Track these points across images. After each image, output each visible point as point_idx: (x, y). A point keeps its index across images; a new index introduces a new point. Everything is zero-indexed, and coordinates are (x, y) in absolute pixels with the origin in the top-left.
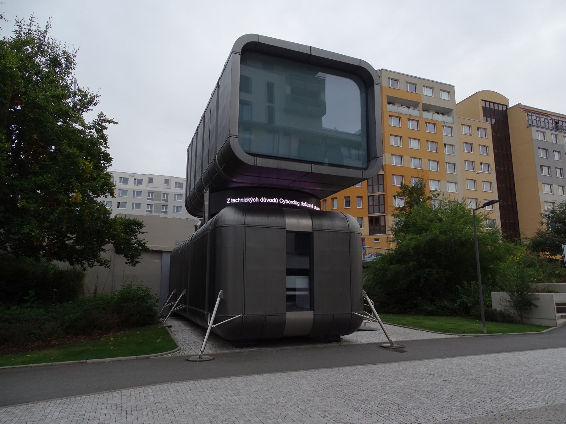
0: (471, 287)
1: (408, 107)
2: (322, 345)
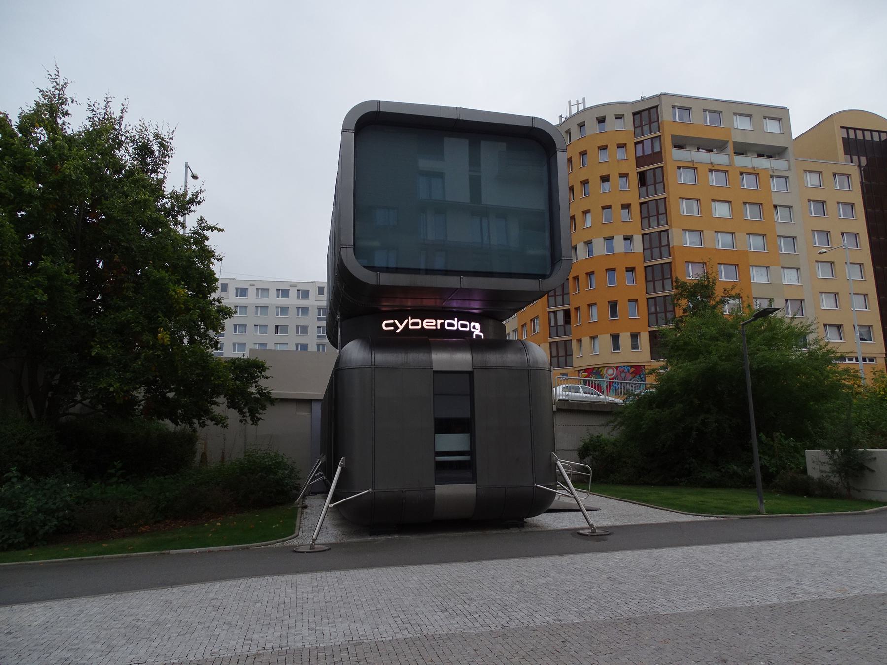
0: (773, 441)
1: (709, 150)
2: (494, 532)
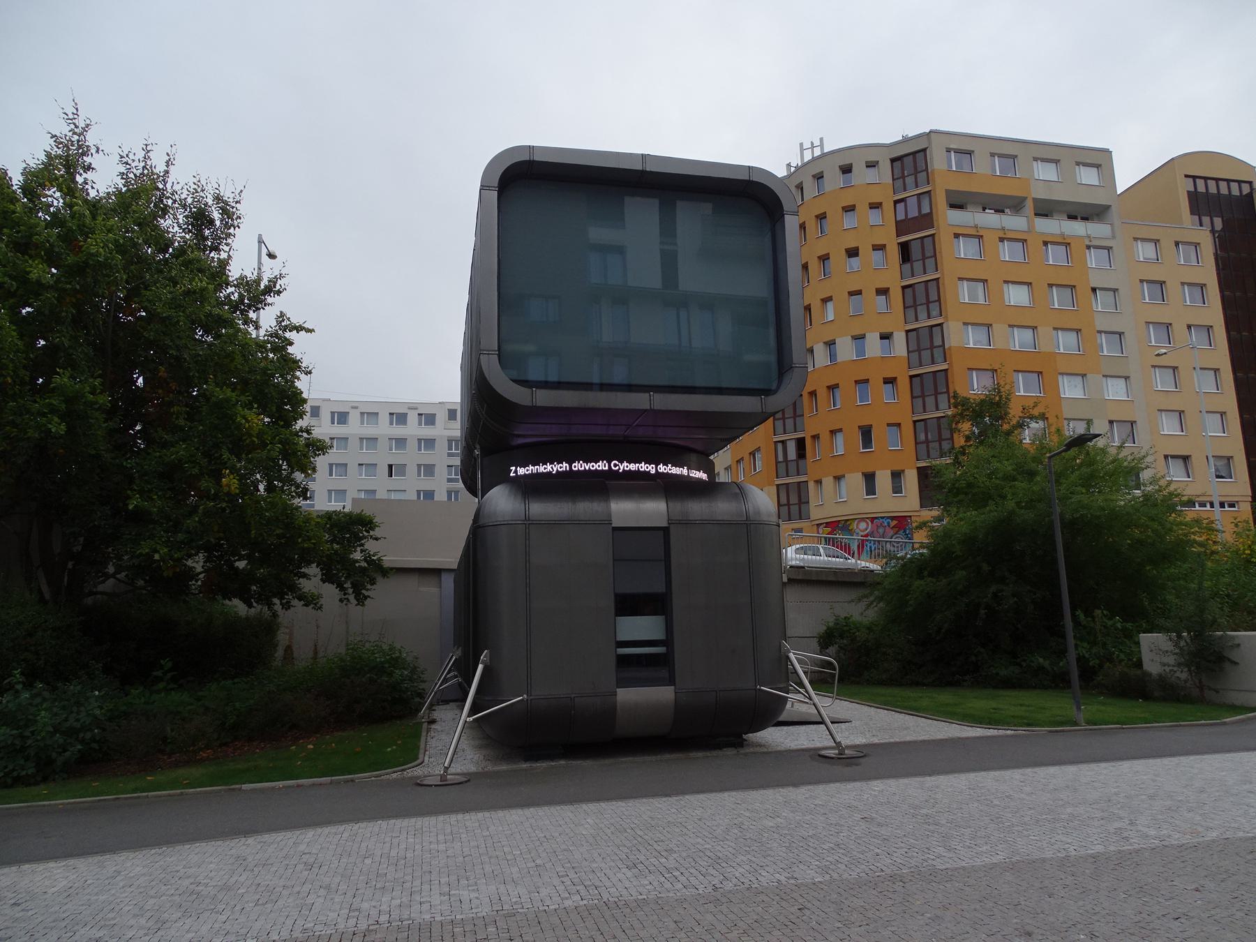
1: (1000, 211)
2: (700, 754)
